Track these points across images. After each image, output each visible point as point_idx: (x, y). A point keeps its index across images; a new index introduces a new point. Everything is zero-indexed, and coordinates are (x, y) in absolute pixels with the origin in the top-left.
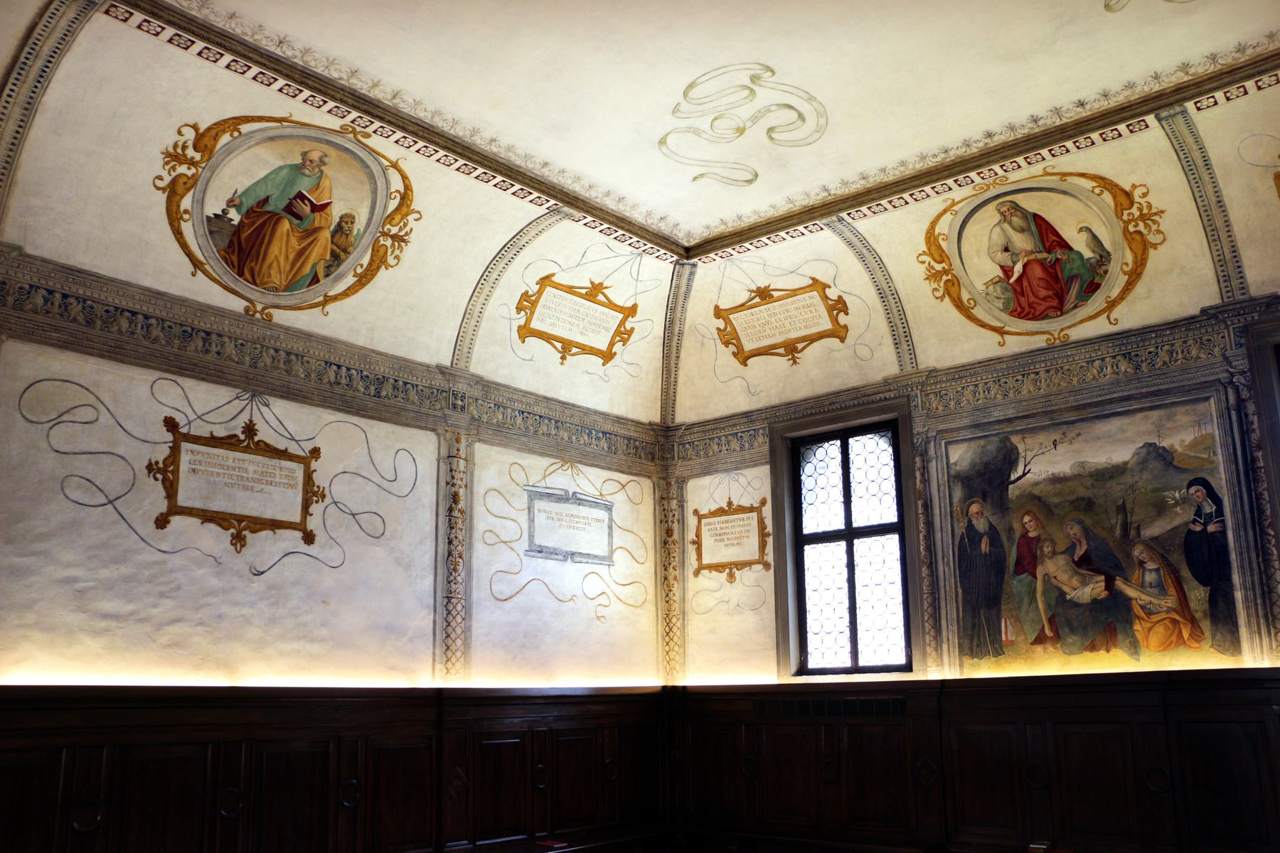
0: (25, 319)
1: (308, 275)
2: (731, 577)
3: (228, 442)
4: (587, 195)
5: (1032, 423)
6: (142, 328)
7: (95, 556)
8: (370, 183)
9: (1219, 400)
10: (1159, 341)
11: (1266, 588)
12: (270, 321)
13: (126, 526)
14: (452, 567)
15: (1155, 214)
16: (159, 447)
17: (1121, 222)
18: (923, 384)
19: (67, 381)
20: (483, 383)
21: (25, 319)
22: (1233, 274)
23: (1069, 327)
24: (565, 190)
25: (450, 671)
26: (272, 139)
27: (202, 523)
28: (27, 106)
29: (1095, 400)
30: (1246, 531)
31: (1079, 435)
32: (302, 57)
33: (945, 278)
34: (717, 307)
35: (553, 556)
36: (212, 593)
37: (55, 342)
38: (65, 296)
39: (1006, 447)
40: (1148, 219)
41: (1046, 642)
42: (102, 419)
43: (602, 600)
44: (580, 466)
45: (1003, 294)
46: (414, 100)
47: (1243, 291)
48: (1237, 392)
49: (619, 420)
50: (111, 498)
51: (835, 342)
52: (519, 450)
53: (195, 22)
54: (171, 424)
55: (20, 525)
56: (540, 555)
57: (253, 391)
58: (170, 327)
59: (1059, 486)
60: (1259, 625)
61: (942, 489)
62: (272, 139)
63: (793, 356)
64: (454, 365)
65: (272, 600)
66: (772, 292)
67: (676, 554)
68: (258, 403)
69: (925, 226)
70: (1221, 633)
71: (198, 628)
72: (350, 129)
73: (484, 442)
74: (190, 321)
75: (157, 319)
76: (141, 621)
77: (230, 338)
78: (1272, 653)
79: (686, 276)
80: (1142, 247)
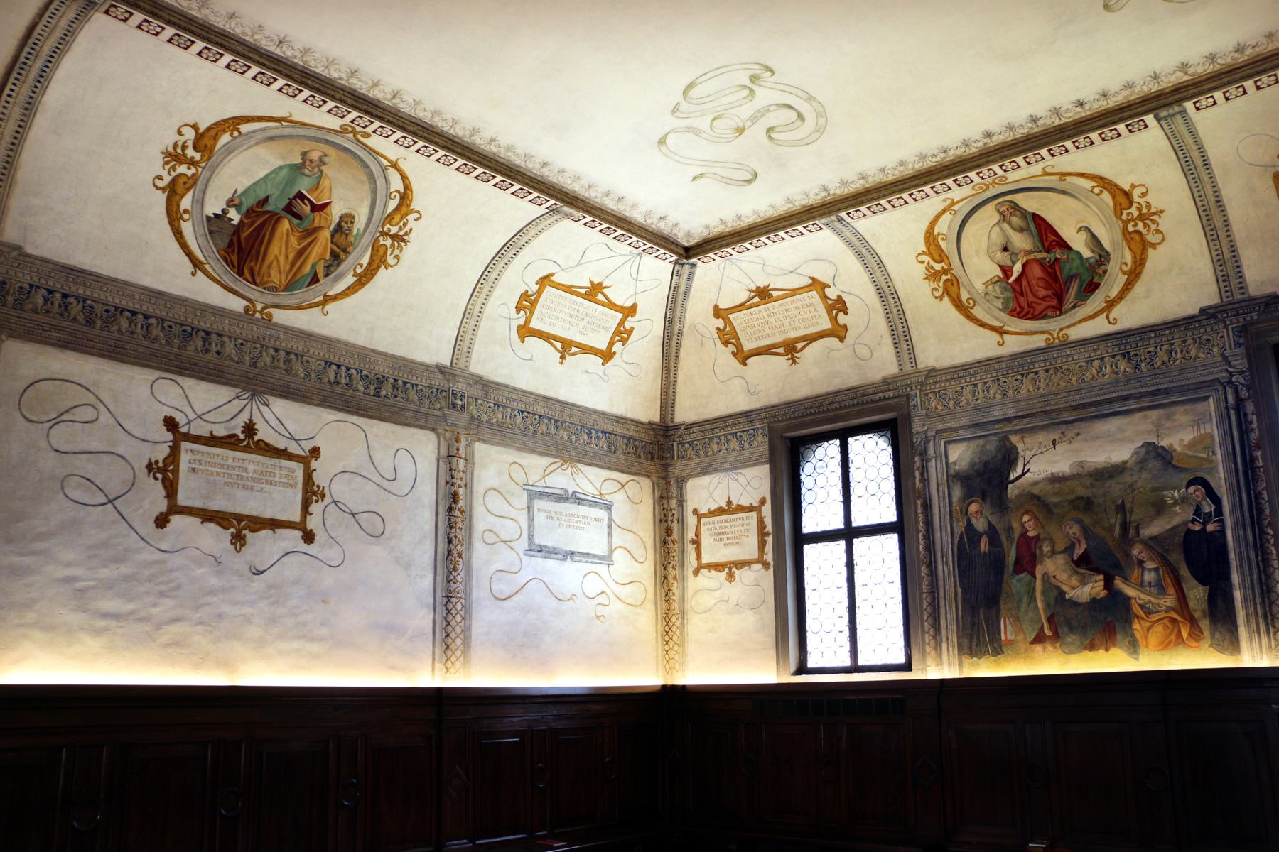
0: (25, 319)
1: (308, 274)
2: (731, 576)
3: (228, 442)
4: (587, 195)
5: (1031, 423)
6: (142, 327)
7: (95, 556)
8: (370, 183)
9: (1218, 399)
10: (1158, 340)
11: (1265, 588)
12: (270, 320)
13: (126, 525)
14: (452, 566)
15: (1155, 214)
16: (159, 447)
17: (1120, 222)
18: (922, 384)
19: (67, 381)
20: (483, 382)
21: (25, 319)
22: (1232, 274)
23: (1068, 327)
24: (565, 190)
25: (450, 670)
26: (272, 139)
27: (202, 523)
28: (27, 106)
29: (1094, 399)
30: (1245, 530)
31: (1078, 434)
32: (302, 57)
33: (944, 278)
34: (716, 307)
35: (552, 555)
36: (212, 592)
37: (55, 341)
38: (65, 296)
39: (1005, 446)
40: (1147, 219)
41: (1045, 642)
42: (102, 419)
43: (602, 599)
44: (579, 466)
45: (1002, 294)
46: (414, 100)
47: (1242, 291)
48: (1236, 392)
49: (619, 420)
50: (111, 497)
51: (834, 341)
52: (519, 449)
53: (195, 22)
54: (170, 424)
55: (20, 524)
56: (539, 554)
57: (253, 390)
58: (170, 327)
59: (1058, 485)
60: (1258, 624)
61: (941, 488)
62: (272, 139)
63: (793, 355)
64: (454, 365)
65: (272, 599)
66: (771, 292)
67: (676, 554)
68: (258, 403)
69: (924, 226)
70: (1220, 632)
71: (198, 627)
72: (350, 129)
73: (484, 441)
74: (190, 320)
75: (157, 318)
76: (141, 620)
77: (230, 337)
78: (1271, 652)
79: (685, 276)
80: (1141, 246)
